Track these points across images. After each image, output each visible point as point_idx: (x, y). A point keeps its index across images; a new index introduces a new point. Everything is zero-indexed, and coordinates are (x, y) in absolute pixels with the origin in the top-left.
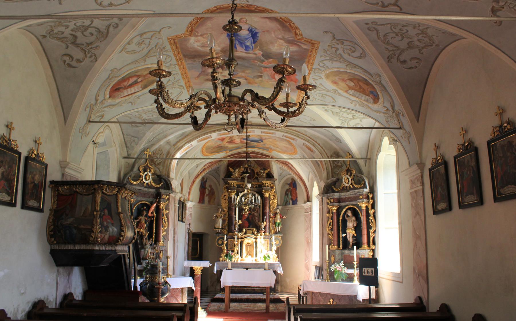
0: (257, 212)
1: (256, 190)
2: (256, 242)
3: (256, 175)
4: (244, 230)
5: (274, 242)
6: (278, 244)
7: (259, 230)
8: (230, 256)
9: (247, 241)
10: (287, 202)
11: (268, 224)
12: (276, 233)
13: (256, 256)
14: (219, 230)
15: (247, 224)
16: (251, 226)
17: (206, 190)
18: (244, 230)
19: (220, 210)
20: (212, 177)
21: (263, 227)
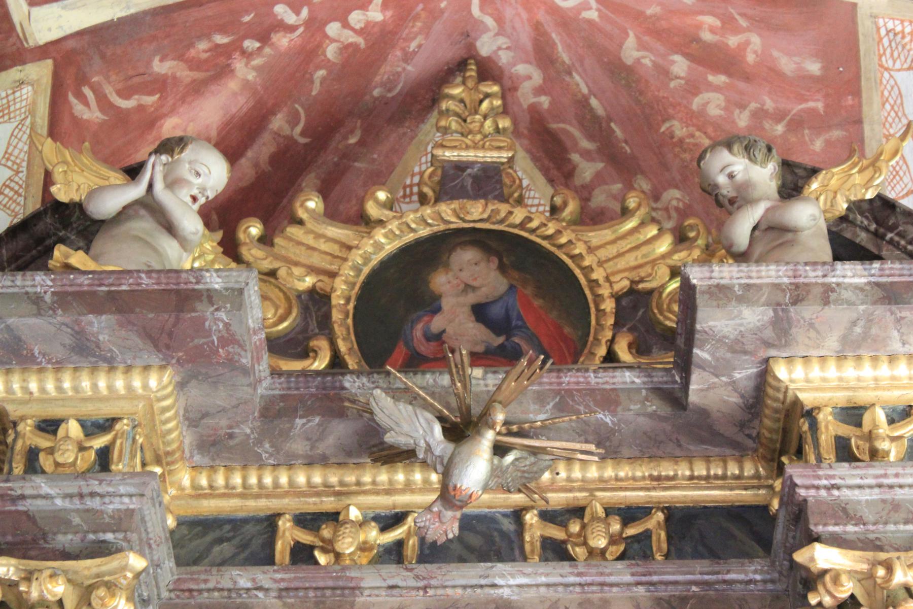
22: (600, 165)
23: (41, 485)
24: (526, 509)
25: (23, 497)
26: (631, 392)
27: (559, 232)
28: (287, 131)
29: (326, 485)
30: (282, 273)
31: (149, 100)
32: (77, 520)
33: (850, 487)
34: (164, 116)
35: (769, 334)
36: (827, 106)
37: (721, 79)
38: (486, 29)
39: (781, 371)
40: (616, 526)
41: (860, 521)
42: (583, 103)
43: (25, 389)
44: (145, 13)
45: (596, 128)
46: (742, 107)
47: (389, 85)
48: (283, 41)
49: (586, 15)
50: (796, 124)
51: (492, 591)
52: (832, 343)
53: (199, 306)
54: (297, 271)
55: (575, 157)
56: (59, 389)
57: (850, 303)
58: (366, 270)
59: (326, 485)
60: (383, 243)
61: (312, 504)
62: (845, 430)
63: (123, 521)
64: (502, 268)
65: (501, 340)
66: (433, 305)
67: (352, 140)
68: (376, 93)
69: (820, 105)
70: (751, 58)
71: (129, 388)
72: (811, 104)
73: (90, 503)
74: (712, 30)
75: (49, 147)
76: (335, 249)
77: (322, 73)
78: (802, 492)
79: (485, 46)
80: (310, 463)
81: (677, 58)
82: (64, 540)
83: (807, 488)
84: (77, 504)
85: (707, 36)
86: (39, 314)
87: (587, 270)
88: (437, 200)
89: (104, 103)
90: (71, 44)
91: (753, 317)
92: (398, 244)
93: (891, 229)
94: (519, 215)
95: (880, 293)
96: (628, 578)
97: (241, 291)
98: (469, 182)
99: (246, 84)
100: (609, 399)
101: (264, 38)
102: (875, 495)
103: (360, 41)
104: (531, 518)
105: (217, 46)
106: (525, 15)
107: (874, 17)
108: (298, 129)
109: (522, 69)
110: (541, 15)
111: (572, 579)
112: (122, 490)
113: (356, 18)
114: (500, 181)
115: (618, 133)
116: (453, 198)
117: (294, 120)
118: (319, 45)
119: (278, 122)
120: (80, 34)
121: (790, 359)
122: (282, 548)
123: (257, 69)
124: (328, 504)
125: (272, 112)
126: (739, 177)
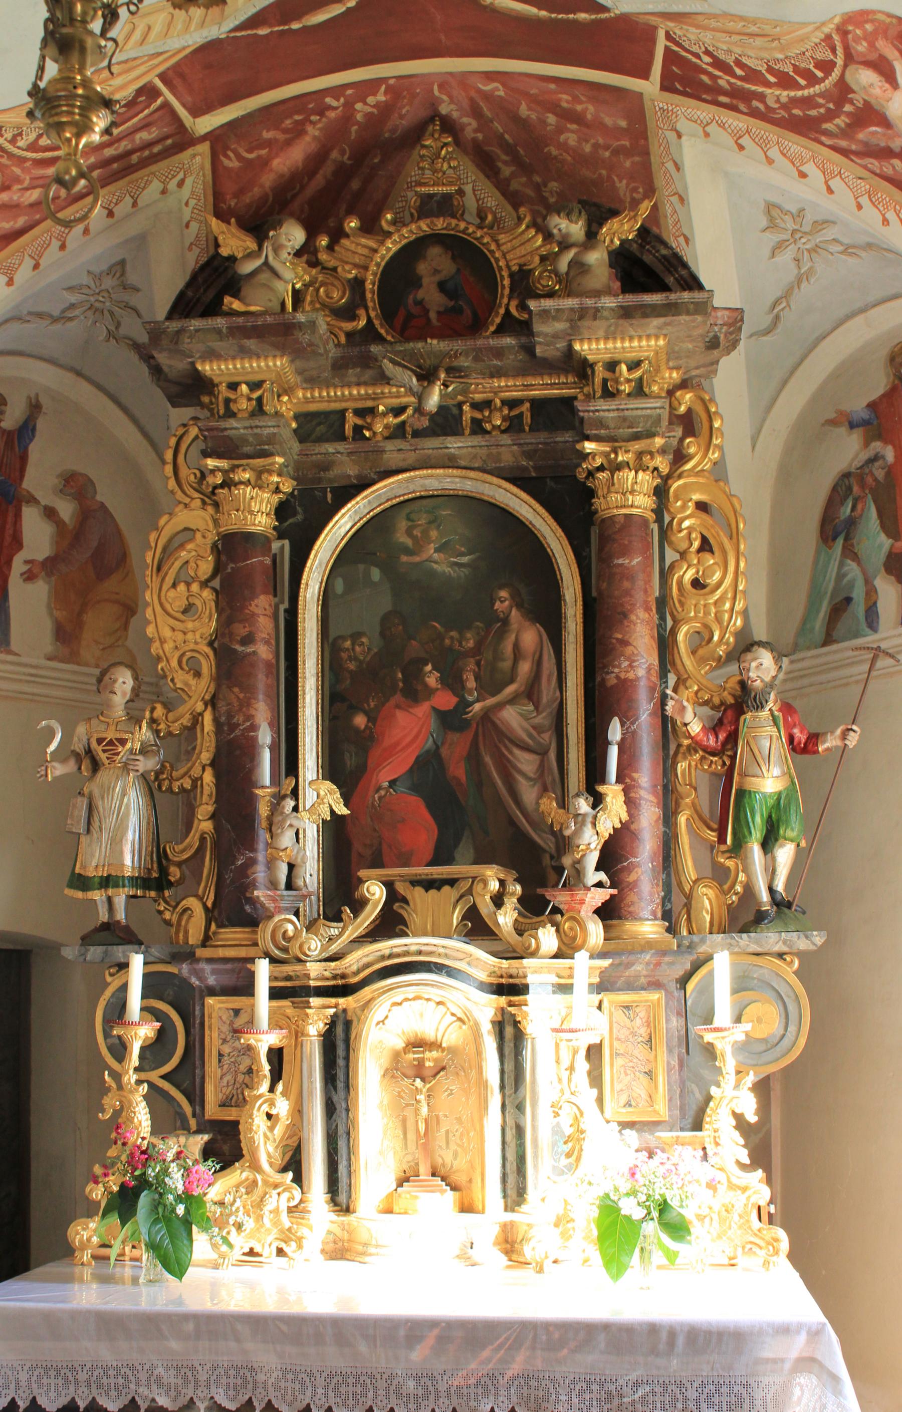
0: (531, 693)
1: (509, 451)
2: (510, 1035)
3: (506, 302)
4: (375, 892)
5: (727, 1034)
6: (770, 1045)
7: (540, 876)
8: (161, 1213)
9: (391, 1020)
10: (841, 606)
11: (649, 816)
12: (744, 917)
13: (515, 1190)
14: (120, 899)
15: (420, 826)
16: (465, 849)
17: (30, 517)
18: (375, 892)
19: (124, 682)
20: (84, 393)
21: (590, 843)
22: (513, 168)
23: (233, 423)
24: (464, 403)
25: (226, 429)
26: (511, 347)
27: (482, 237)
28: (339, 158)
29: (367, 394)
30: (340, 269)
31: (264, 152)
32: (251, 439)
33: (604, 411)
34: (273, 158)
35: (569, 331)
36: (631, 144)
37: (574, 127)
38: (444, 101)
39: (577, 347)
40: (506, 411)
41: (607, 428)
42: (501, 137)
43: (220, 369)
44: (255, 111)
45: (509, 149)
46: (587, 141)
47: (393, 131)
48: (332, 115)
49: (497, 93)
50: (616, 152)
51: (446, 451)
52: (601, 333)
53: (296, 332)
54: (347, 267)
55: (500, 164)
56: (235, 368)
57: (607, 319)
58: (383, 264)
59: (367, 394)
60: (391, 247)
61: (360, 405)
62: (608, 375)
63: (271, 439)
64: (453, 258)
65: (452, 303)
66: (416, 282)
67: (376, 161)
68: (386, 135)
69: (627, 143)
70: (589, 117)
71: (267, 366)
72: (623, 142)
73: (258, 431)
74: (567, 102)
75: (214, 222)
76: (365, 252)
77: (355, 128)
78: (581, 414)
79: (444, 109)
80: (358, 384)
81: (550, 115)
82: (247, 449)
83: (584, 411)
84: (250, 431)
85: (565, 105)
86: (221, 340)
87: (497, 260)
88: (419, 218)
89: (239, 157)
90: (218, 132)
91: (560, 326)
92: (399, 246)
93: (648, 244)
94: (462, 225)
95: (622, 312)
96: (509, 442)
97: (314, 322)
98: (435, 206)
99: (315, 138)
100: (499, 353)
101: (321, 114)
102: (615, 414)
103: (375, 111)
104: (466, 408)
105: (296, 121)
106: (463, 94)
107: (653, 101)
108: (346, 157)
109: (465, 120)
110: (473, 94)
111: (483, 443)
112: (270, 424)
113: (371, 100)
114: (452, 205)
115: (522, 152)
116: (427, 217)
117: (343, 153)
118: (352, 114)
119: (335, 155)
120: (222, 126)
121: (582, 340)
122: (348, 429)
123: (320, 129)
124: (369, 404)
125: (332, 149)
126: (564, 231)
